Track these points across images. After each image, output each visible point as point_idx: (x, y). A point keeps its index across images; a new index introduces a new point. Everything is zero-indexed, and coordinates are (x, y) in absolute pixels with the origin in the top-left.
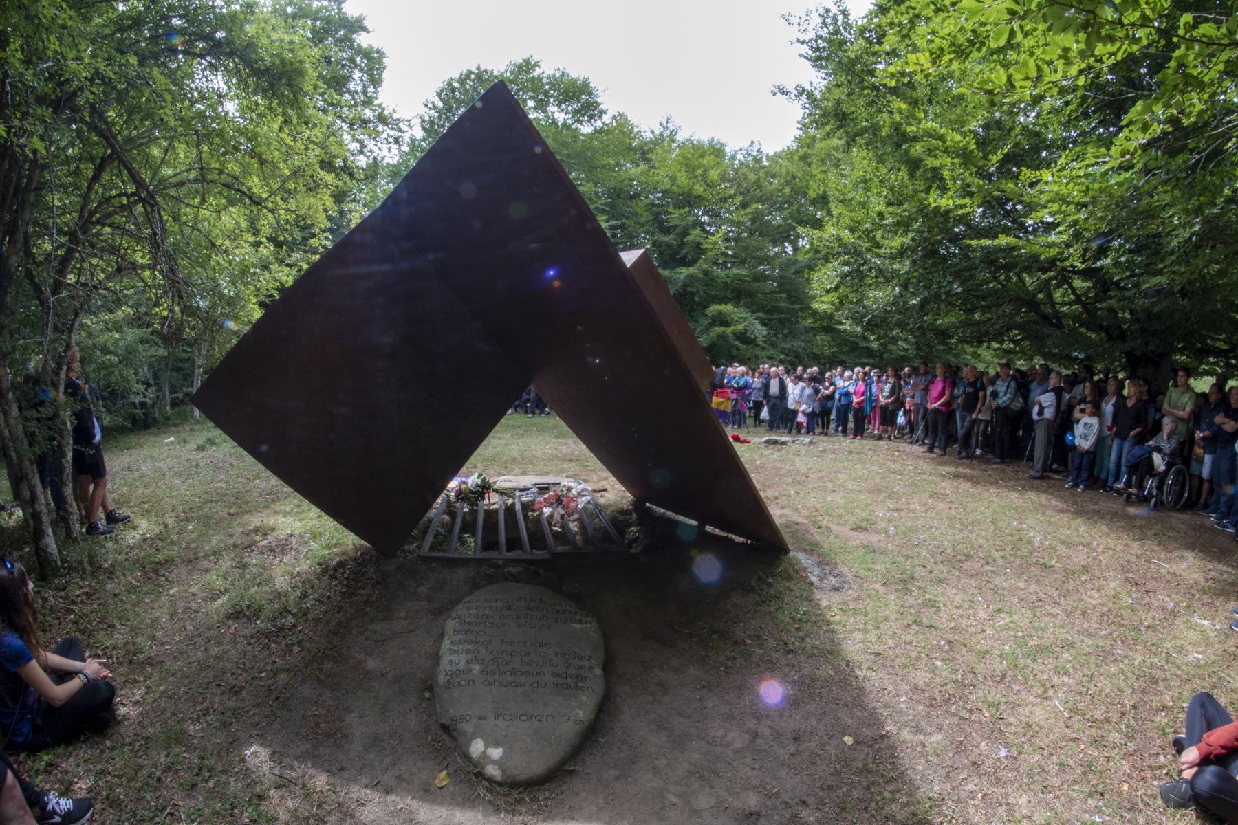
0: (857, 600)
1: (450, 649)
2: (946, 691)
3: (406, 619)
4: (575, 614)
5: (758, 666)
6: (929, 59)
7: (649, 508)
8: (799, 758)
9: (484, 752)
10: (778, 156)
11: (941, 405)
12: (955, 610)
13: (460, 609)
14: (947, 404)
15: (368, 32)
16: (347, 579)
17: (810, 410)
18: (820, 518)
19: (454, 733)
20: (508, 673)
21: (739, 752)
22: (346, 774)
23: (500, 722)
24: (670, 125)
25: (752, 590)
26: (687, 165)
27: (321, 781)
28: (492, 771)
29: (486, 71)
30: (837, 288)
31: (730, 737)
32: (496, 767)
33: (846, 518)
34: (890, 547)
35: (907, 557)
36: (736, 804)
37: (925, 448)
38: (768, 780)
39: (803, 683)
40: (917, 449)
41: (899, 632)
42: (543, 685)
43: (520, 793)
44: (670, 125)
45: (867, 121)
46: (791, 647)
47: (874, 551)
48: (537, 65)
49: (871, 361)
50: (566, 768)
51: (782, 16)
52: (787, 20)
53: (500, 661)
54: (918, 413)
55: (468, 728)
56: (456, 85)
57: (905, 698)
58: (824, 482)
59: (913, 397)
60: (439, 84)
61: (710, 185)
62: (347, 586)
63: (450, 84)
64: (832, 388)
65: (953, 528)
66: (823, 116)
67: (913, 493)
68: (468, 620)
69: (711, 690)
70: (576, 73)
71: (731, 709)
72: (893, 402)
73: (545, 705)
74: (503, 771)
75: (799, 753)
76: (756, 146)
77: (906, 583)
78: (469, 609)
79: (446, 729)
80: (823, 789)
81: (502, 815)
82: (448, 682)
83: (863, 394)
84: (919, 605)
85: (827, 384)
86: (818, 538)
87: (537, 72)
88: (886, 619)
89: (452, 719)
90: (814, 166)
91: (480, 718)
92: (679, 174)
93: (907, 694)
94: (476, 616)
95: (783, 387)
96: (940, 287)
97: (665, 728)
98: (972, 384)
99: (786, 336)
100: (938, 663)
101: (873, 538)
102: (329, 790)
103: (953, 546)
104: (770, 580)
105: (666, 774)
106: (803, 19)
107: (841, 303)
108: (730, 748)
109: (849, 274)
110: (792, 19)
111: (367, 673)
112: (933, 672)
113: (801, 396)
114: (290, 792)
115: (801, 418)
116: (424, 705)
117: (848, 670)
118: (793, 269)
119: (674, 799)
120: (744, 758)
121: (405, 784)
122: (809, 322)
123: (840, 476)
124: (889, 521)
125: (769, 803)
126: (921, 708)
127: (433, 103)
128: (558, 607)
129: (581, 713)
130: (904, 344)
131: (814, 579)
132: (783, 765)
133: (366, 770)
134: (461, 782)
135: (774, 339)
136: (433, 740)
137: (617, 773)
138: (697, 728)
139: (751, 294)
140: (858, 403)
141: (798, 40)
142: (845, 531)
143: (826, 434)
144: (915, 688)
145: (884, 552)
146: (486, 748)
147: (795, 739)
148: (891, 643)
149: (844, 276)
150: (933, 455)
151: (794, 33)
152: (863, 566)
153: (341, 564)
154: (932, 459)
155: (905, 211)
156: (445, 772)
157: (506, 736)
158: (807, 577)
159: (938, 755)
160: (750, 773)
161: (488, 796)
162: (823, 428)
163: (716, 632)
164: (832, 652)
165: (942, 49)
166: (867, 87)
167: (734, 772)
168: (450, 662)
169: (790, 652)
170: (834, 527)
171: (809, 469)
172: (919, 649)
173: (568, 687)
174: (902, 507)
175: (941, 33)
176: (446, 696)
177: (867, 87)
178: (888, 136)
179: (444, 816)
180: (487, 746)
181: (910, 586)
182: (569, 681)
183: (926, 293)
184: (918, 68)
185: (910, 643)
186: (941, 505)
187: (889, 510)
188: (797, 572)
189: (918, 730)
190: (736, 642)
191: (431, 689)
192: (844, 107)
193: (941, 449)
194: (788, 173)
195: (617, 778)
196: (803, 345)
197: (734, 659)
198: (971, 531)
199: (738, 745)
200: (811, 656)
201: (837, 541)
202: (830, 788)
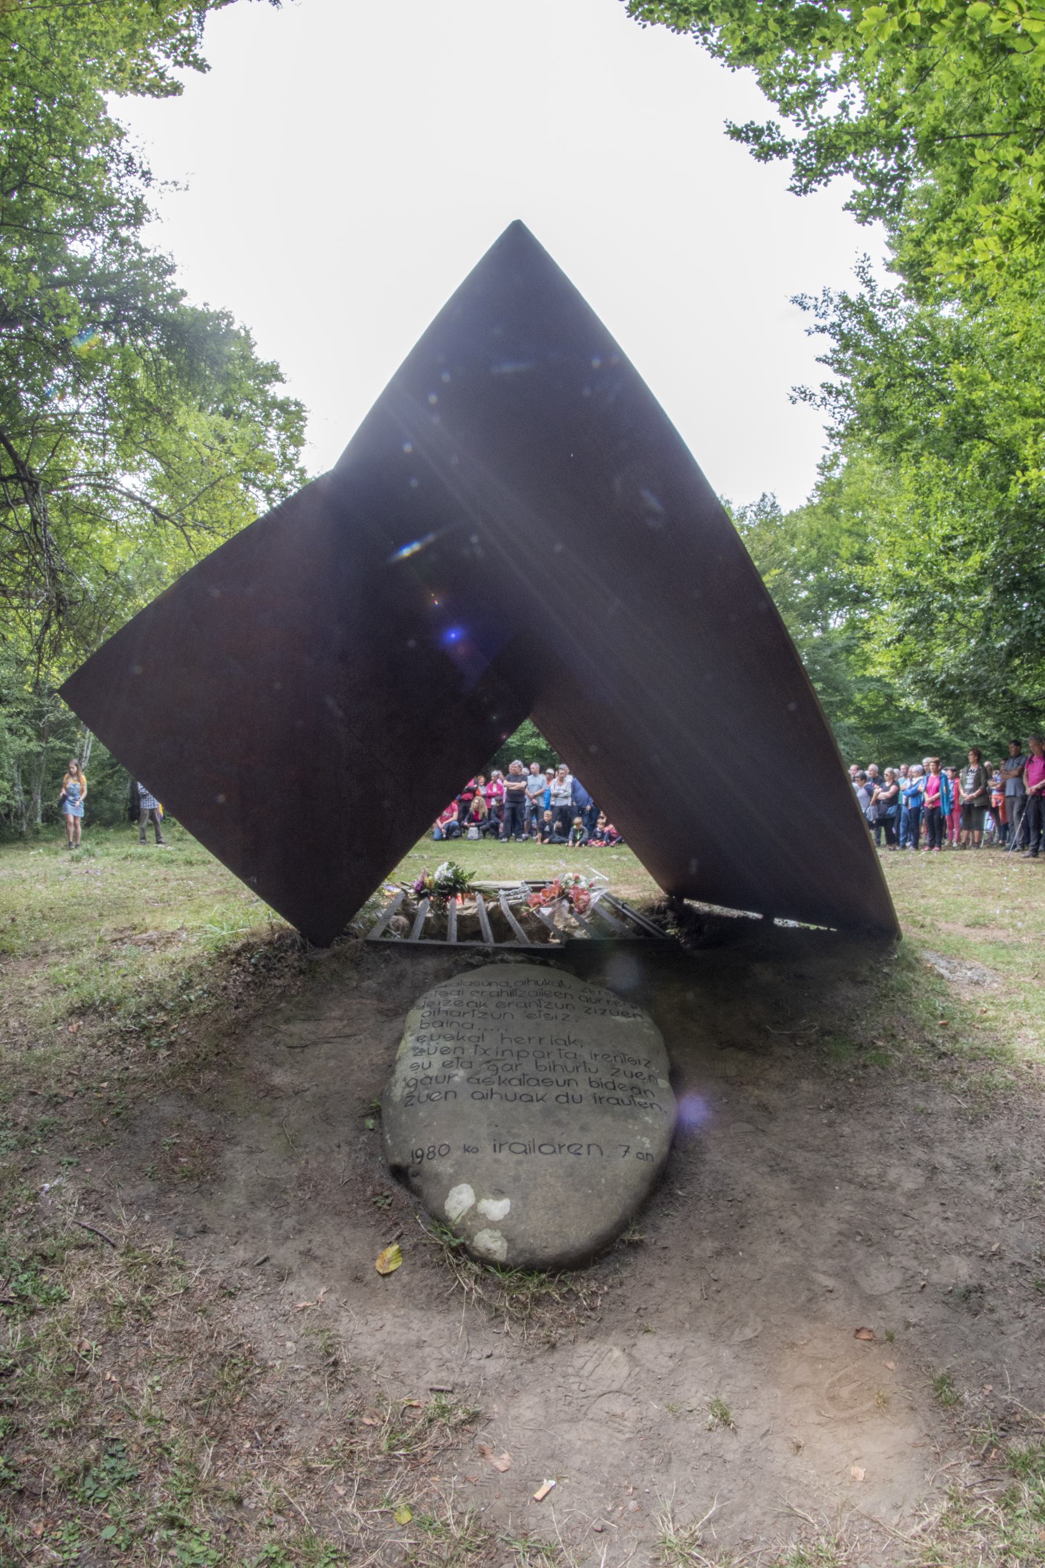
3: (341, 1019)
8: (1011, 1194)
9: (474, 1208)
13: (433, 995)
16: (255, 965)
19: (416, 1181)
21: (914, 1196)
22: (209, 1240)
23: (504, 1155)
25: (864, 982)
27: (163, 1247)
30: (900, 639)
31: (892, 1174)
32: (498, 1234)
36: (935, 1278)
42: (577, 1098)
43: (542, 1284)
45: (915, 418)
46: (943, 1049)
50: (627, 1236)
52: (800, 304)
55: (443, 1167)
62: (253, 974)
64: (893, 788)
68: (443, 1008)
69: (841, 1110)
71: (881, 1135)
72: (979, 796)
73: (584, 1128)
74: (510, 1241)
75: (1009, 1187)
79: (400, 1174)
81: (506, 1326)
82: (410, 1096)
83: (937, 790)
85: (887, 784)
89: (414, 1155)
91: (466, 1149)
96: (1032, 623)
105: (804, 1241)
106: (820, 300)
108: (899, 1190)
111: (271, 1092)
116: (363, 1138)
117: (1034, 1072)
118: (828, 652)
119: (830, 1283)
120: (926, 1204)
121: (316, 1265)
122: (852, 720)
125: (989, 1269)
128: (588, 994)
133: (247, 1236)
134: (424, 1265)
136: (375, 1195)
137: (716, 1244)
140: (932, 802)
141: (817, 327)
142: (960, 929)
146: (478, 1200)
147: (997, 1168)
151: (810, 319)
153: (247, 947)
156: (396, 1247)
157: (517, 1179)
160: (943, 1227)
163: (829, 1033)
164: (998, 1055)
166: (910, 375)
167: (916, 1227)
168: (414, 1067)
177: (910, 375)
180: (478, 1197)
182: (619, 1094)
191: (377, 1113)
195: (718, 1253)
199: (908, 1185)
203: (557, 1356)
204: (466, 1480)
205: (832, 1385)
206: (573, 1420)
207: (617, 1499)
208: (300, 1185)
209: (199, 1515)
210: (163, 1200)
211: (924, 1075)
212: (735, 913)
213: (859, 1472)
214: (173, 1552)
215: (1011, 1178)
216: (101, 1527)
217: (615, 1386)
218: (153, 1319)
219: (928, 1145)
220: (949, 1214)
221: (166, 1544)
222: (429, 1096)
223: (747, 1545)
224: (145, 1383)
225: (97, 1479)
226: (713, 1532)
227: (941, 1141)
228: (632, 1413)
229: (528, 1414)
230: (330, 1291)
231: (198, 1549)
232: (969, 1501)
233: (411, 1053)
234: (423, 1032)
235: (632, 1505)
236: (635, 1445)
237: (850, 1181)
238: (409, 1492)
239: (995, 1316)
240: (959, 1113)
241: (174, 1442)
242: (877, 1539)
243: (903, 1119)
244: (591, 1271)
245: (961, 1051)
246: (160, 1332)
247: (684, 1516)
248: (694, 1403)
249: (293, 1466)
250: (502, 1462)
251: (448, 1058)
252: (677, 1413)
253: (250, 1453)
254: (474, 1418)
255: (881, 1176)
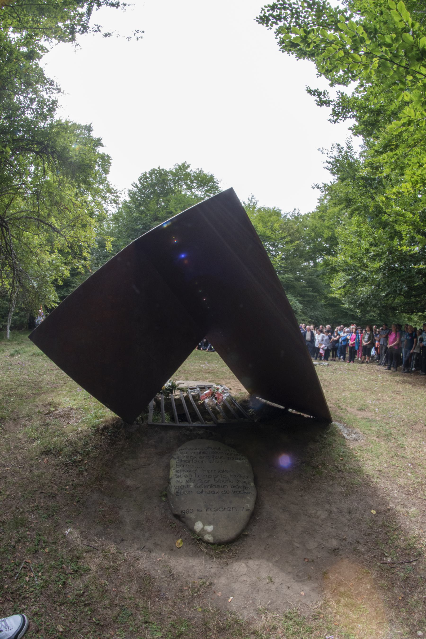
0: (366, 445)
1: (176, 475)
2: (415, 487)
4: (237, 455)
5: (326, 478)
6: (411, 185)
7: (258, 399)
8: (352, 521)
9: (203, 528)
10: (307, 216)
11: (395, 345)
12: (413, 449)
14: (398, 345)
15: (103, 146)
17: (326, 348)
18: (341, 404)
19: (183, 519)
20: (209, 487)
21: (324, 520)
22: (125, 543)
23: (209, 512)
24: (253, 200)
26: (263, 221)
27: (112, 548)
28: (208, 538)
29: (163, 170)
30: (344, 287)
31: (319, 513)
32: (210, 535)
33: (354, 404)
34: (377, 418)
35: (387, 424)
37: (386, 367)
38: (340, 533)
39: (348, 486)
40: (382, 368)
41: (388, 460)
43: (223, 548)
44: (253, 200)
45: (361, 203)
46: (340, 469)
47: (370, 421)
48: (188, 167)
49: (355, 322)
51: (319, 150)
52: (321, 151)
53: (203, 480)
54: (382, 349)
55: (192, 516)
56: (148, 175)
57: (396, 491)
58: (339, 386)
59: (379, 341)
60: (139, 175)
61: (274, 231)
63: (145, 175)
64: (338, 337)
65: (406, 408)
66: (339, 200)
67: (384, 391)
70: (207, 171)
72: (369, 344)
73: (231, 502)
74: (214, 537)
75: (352, 519)
76: (297, 211)
77: (387, 436)
78: (183, 453)
79: (177, 516)
80: (365, 535)
81: (215, 560)
82: (177, 492)
83: (354, 340)
84: (395, 447)
86: (342, 414)
87: (188, 170)
88: (382, 454)
89: (182, 512)
90: (326, 221)
91: (198, 511)
92: (259, 225)
93: (397, 489)
94: (187, 457)
95: (313, 336)
96: (396, 287)
97: (287, 511)
98: (411, 335)
99: (311, 309)
100: (409, 474)
101: (369, 414)
102: (118, 552)
103: (408, 418)
104: (325, 436)
107: (346, 294)
109: (351, 280)
110: (324, 151)
112: (407, 478)
113: (322, 340)
114: (95, 554)
115: (321, 351)
116: (162, 504)
117: (368, 479)
119: (298, 545)
121: (159, 547)
123: (347, 383)
124: (375, 406)
125: (342, 543)
126: (404, 495)
127: (136, 184)
129: (248, 505)
130: (373, 314)
131: (345, 435)
132: (345, 525)
133: (136, 540)
134: (189, 544)
135: (305, 310)
138: (302, 510)
139: (293, 287)
140: (352, 344)
142: (355, 411)
143: (335, 360)
144: (400, 486)
145: (375, 421)
147: (349, 513)
148: (385, 465)
149: (348, 281)
150: (391, 371)
152: (366, 428)
154: (390, 373)
155: (381, 249)
156: (181, 540)
157: (214, 519)
158: (342, 434)
159: (415, 517)
160: (331, 530)
161: (206, 551)
162: (333, 357)
164: (358, 471)
165: (417, 181)
168: (177, 482)
169: (340, 471)
170: (348, 409)
171: (330, 379)
172: (399, 468)
173: (240, 492)
174: (380, 398)
175: (417, 174)
176: (177, 500)
178: (372, 211)
179: (183, 563)
180: (204, 525)
181: (390, 438)
182: (240, 490)
183: (389, 290)
184: (406, 190)
185: (395, 465)
186: (399, 397)
187: (374, 400)
188: (337, 432)
189: (404, 506)
190: (314, 467)
191: (166, 496)
192: (350, 196)
193: (394, 368)
194: (313, 225)
195: (268, 537)
196: (320, 314)
197: (314, 475)
198: (415, 410)
199: (323, 517)
200: (349, 473)
201: (351, 416)
202: (369, 535)
203: (229, 566)
204: (212, 599)
205: (297, 572)
206: (235, 582)
207: (247, 600)
208: (147, 522)
209: (151, 618)
210: (106, 532)
211: (333, 478)
212: (298, 413)
213: (303, 593)
214: (149, 629)
215: (353, 516)
216: (129, 628)
217: (244, 573)
218: (118, 570)
219: (330, 504)
220: (333, 527)
221: (146, 628)
222: (184, 493)
223: (277, 609)
224: (125, 589)
225: (122, 617)
226: (270, 607)
227: (334, 503)
228: (249, 580)
229: (224, 582)
230: (165, 554)
231: (155, 627)
232: (328, 601)
233: (175, 477)
234: (178, 469)
235: (251, 601)
236: (250, 588)
237: (306, 515)
238: (199, 604)
239: (341, 557)
240: (342, 493)
241: (139, 602)
242: (307, 609)
243: (324, 494)
244: (235, 544)
245: (346, 470)
246: (122, 574)
247: (263, 603)
248: (264, 577)
249: (170, 602)
250: (219, 594)
251: (187, 479)
252: (260, 579)
253: (158, 601)
254: (211, 584)
255: (315, 514)
